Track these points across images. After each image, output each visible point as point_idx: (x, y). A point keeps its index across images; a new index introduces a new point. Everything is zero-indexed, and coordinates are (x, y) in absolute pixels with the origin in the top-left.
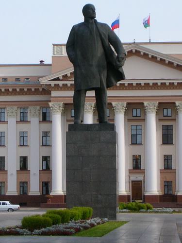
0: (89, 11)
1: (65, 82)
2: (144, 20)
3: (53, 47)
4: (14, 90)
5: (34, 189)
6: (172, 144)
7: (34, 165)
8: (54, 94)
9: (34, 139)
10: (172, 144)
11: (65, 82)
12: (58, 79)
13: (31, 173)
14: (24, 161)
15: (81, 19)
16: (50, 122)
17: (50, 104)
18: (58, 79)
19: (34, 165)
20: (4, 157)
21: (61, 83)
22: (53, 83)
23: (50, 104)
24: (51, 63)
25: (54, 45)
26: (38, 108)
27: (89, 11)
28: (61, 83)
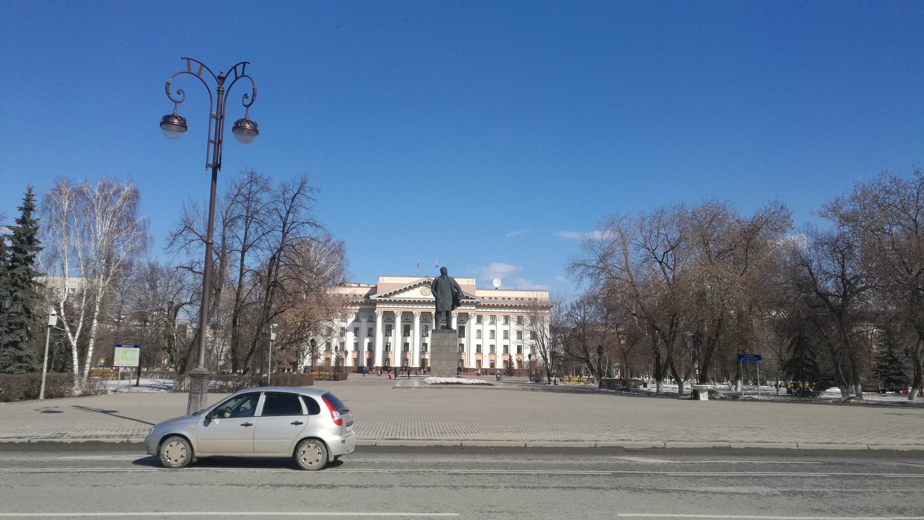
1: (385, 299)
5: (396, 362)
7: (486, 350)
12: (381, 297)
17: (376, 311)
22: (378, 299)
23: (376, 311)
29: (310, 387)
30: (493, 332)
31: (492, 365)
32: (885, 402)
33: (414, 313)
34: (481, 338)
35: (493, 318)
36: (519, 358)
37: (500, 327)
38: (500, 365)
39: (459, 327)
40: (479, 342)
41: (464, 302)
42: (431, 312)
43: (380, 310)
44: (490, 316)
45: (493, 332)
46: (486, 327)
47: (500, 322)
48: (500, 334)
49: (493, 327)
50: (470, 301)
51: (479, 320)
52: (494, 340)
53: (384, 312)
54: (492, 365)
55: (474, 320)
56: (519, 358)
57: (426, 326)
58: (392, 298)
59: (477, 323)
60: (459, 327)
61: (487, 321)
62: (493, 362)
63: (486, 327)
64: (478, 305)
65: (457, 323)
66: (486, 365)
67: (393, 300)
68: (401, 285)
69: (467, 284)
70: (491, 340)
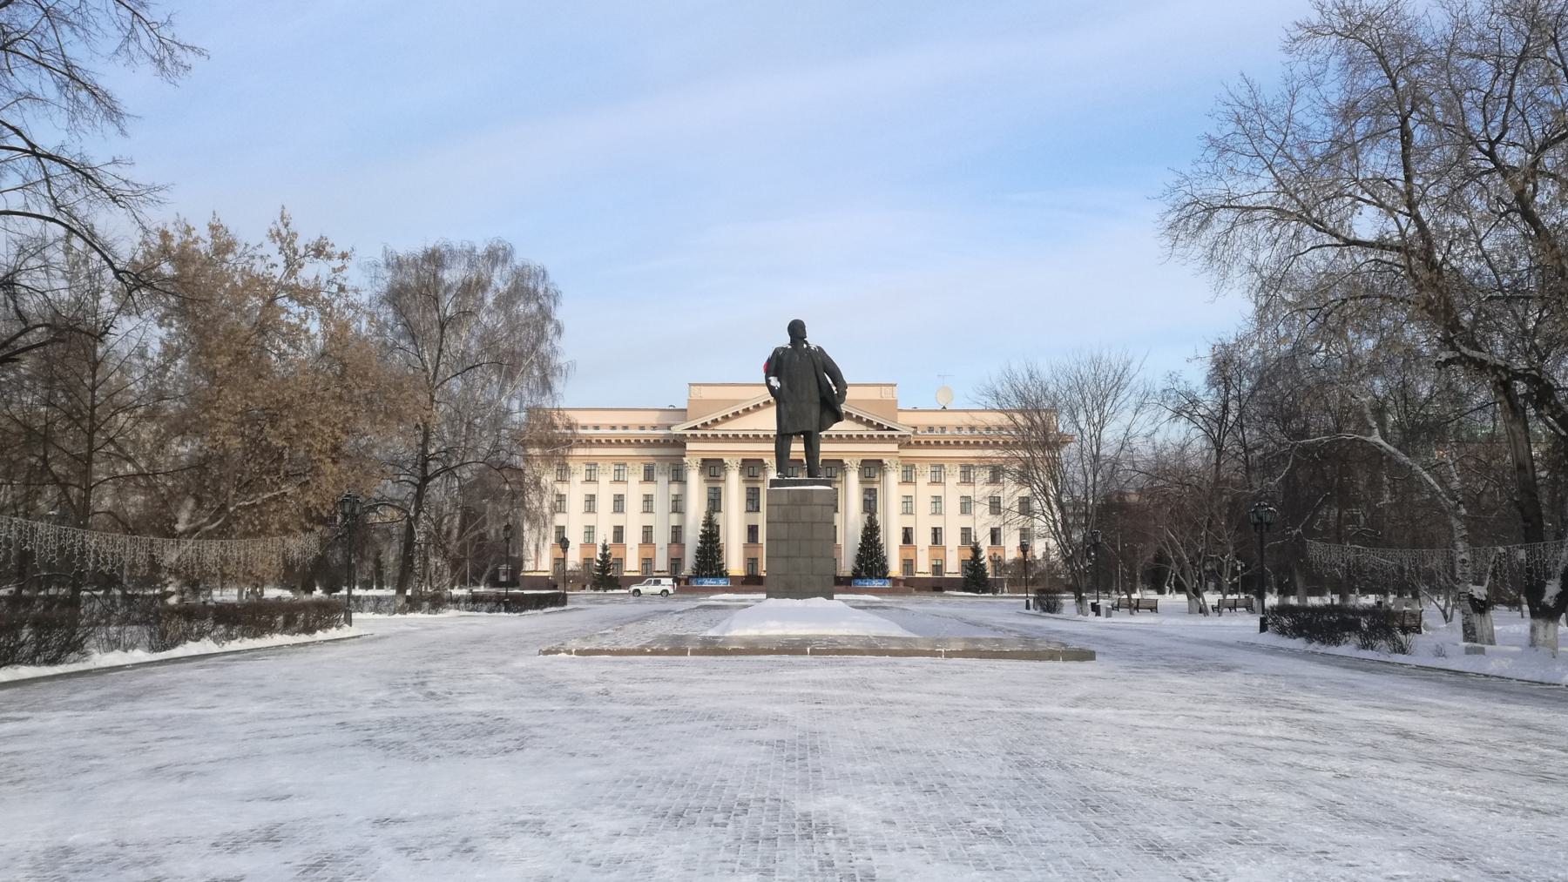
0: (797, 330)
1: (704, 432)
2: (559, 330)
3: (690, 390)
4: (986, 443)
5: (923, 568)
6: (622, 511)
7: (923, 539)
8: (690, 446)
9: (923, 505)
10: (564, 512)
11: (704, 432)
12: (695, 428)
13: (628, 547)
14: (936, 534)
15: (785, 340)
16: (685, 482)
17: (685, 459)
18: (695, 428)
19: (923, 539)
20: (564, 527)
21: (699, 433)
22: (689, 433)
23: (685, 459)
24: (685, 407)
25: (690, 385)
26: (667, 464)
27: (797, 330)
28: (699, 433)
29: (1055, 615)
30: (937, 500)
31: (937, 568)
32: (833, 640)
33: (845, 462)
34: (911, 514)
35: (938, 469)
36: (995, 554)
37: (953, 489)
38: (953, 568)
39: (866, 489)
40: (908, 521)
41: (872, 436)
42: (881, 461)
43: (696, 450)
44: (961, 466)
45: (937, 500)
46: (923, 490)
47: (953, 478)
48: (605, 503)
49: (937, 490)
50: (886, 434)
51: (908, 479)
52: (942, 518)
53: (744, 460)
54: (937, 568)
55: (894, 477)
56: (995, 554)
57: (715, 488)
58: (721, 429)
59: (645, 480)
60: (748, 488)
61: (923, 481)
62: (939, 563)
63: (923, 490)
64: (905, 443)
65: (861, 482)
66: (923, 568)
67: (720, 434)
68: (736, 402)
69: (879, 398)
70: (935, 517)
